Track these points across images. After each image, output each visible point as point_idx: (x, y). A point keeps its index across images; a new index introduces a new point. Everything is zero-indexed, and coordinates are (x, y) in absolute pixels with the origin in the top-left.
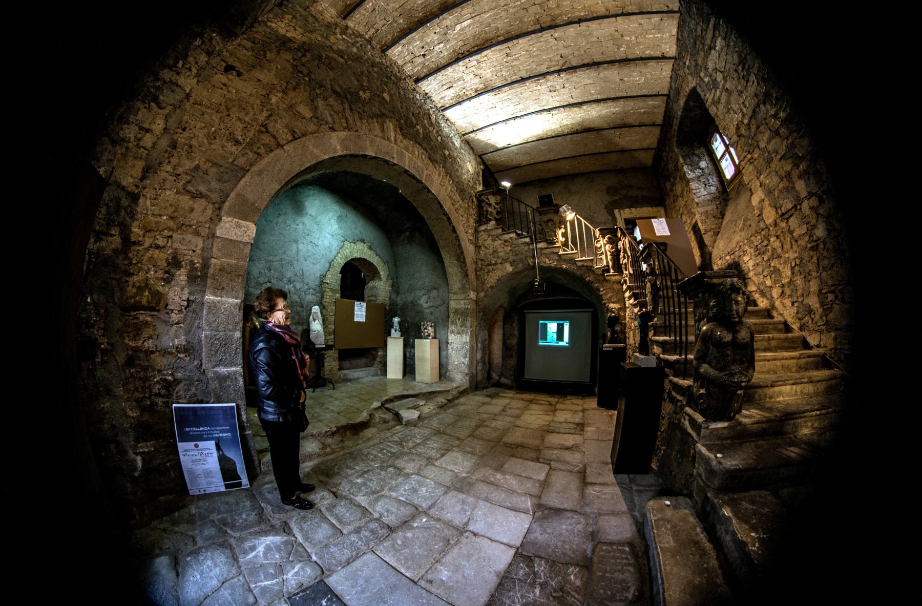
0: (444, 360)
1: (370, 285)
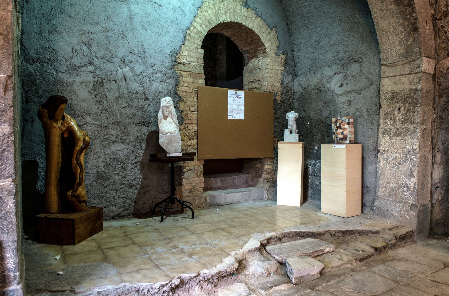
0: (369, 181)
1: (252, 64)
